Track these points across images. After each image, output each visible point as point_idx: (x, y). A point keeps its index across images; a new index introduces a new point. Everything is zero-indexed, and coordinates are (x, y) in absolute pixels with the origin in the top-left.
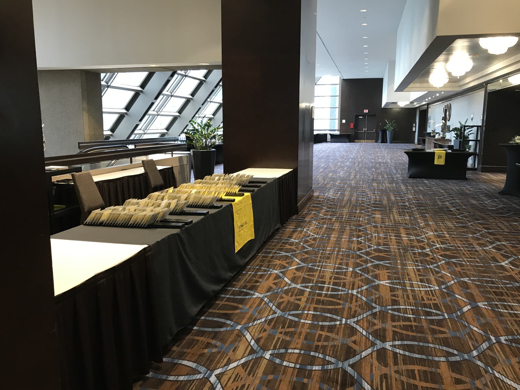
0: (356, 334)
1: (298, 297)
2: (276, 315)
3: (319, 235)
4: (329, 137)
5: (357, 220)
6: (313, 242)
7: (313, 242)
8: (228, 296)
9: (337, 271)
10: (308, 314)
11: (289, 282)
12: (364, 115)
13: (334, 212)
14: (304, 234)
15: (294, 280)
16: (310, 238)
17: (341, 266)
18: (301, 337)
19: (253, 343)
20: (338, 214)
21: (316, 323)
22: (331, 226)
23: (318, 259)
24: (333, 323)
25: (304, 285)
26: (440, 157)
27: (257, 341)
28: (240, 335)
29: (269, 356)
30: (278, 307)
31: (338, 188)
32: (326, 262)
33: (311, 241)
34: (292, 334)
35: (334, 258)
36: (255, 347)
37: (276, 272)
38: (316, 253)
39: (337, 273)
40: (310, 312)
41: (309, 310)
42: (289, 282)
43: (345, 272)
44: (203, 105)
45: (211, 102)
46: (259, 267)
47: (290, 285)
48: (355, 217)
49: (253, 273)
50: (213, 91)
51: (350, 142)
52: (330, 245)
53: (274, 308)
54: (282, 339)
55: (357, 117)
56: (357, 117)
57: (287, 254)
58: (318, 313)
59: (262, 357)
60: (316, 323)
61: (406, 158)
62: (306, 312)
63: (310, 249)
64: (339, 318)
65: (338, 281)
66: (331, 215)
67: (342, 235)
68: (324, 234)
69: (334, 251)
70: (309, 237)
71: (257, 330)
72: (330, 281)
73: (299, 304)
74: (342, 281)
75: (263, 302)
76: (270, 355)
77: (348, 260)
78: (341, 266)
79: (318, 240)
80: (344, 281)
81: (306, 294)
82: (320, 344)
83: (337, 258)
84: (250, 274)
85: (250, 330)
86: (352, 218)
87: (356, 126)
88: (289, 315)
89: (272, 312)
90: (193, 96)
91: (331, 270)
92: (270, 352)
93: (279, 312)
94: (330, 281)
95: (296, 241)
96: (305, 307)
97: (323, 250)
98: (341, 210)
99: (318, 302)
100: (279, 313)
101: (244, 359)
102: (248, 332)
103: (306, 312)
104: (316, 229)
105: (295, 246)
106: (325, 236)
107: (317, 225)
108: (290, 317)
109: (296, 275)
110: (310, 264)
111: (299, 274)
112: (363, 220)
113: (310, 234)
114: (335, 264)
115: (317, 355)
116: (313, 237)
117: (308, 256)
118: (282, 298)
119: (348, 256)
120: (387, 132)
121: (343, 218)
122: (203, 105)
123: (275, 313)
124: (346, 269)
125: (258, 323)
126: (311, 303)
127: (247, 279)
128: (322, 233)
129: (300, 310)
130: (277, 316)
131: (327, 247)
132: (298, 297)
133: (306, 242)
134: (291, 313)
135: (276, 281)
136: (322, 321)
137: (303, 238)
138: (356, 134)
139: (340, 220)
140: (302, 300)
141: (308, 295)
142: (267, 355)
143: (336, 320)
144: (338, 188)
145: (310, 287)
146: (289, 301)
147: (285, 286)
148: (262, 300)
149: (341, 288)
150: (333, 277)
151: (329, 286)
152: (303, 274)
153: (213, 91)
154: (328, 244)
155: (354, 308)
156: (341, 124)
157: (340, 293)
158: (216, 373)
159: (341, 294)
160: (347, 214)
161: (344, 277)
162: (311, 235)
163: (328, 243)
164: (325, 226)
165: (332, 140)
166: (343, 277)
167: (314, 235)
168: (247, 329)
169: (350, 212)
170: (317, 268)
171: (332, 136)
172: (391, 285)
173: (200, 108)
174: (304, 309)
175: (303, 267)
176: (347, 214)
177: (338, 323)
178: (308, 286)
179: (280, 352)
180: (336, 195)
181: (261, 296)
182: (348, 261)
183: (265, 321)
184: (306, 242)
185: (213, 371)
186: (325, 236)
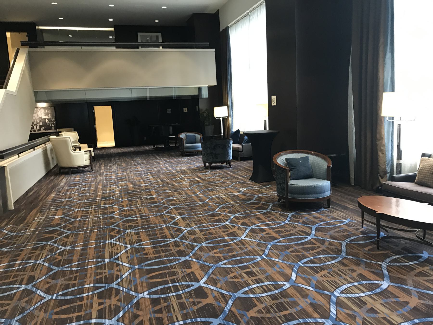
0: (46, 289)
1: (102, 307)
2: (115, 283)
5: (81, 209)
6: (111, 234)
7: (111, 234)
10: (88, 292)
13: (105, 213)
14: (126, 240)
16: (117, 237)
18: (89, 275)
19: (121, 263)
20: (100, 211)
21: (80, 287)
23: (102, 221)
24: (65, 291)
27: (118, 265)
30: (118, 291)
31: (112, 198)
32: (95, 220)
33: (114, 234)
34: (97, 274)
36: (117, 262)
38: (106, 224)
40: (86, 294)
41: (88, 296)
48: (83, 211)
52: (95, 234)
53: (121, 288)
54: (102, 270)
58: (78, 296)
59: (110, 259)
60: (80, 287)
62: (90, 293)
63: (112, 227)
64: (59, 298)
66: (106, 208)
67: (82, 250)
68: (107, 188)
69: (91, 230)
73: (99, 299)
77: (79, 225)
79: (107, 238)
82: (75, 275)
83: (88, 224)
86: (85, 209)
88: (105, 287)
89: (121, 284)
92: (106, 262)
93: (115, 286)
95: (128, 231)
96: (92, 298)
97: (100, 228)
98: (98, 216)
99: (80, 308)
100: (114, 285)
103: (90, 293)
105: (126, 225)
106: (102, 244)
108: (103, 285)
112: (75, 209)
117: (110, 221)
118: (119, 300)
119: (79, 228)
121: (95, 208)
125: (126, 273)
126: (87, 304)
128: (107, 247)
129: (96, 293)
131: (98, 231)
132: (102, 307)
134: (103, 289)
136: (74, 290)
139: (96, 205)
140: (97, 305)
141: (91, 313)
143: (62, 295)
144: (112, 198)
146: (110, 298)
147: (123, 316)
154: (97, 234)
155: (42, 313)
160: (91, 212)
163: (97, 235)
164: (107, 261)
167: (114, 242)
168: (130, 268)
169: (87, 216)
172: (166, 239)
174: (93, 295)
176: (91, 212)
177: (60, 293)
180: (110, 189)
183: (121, 276)
186: (102, 244)
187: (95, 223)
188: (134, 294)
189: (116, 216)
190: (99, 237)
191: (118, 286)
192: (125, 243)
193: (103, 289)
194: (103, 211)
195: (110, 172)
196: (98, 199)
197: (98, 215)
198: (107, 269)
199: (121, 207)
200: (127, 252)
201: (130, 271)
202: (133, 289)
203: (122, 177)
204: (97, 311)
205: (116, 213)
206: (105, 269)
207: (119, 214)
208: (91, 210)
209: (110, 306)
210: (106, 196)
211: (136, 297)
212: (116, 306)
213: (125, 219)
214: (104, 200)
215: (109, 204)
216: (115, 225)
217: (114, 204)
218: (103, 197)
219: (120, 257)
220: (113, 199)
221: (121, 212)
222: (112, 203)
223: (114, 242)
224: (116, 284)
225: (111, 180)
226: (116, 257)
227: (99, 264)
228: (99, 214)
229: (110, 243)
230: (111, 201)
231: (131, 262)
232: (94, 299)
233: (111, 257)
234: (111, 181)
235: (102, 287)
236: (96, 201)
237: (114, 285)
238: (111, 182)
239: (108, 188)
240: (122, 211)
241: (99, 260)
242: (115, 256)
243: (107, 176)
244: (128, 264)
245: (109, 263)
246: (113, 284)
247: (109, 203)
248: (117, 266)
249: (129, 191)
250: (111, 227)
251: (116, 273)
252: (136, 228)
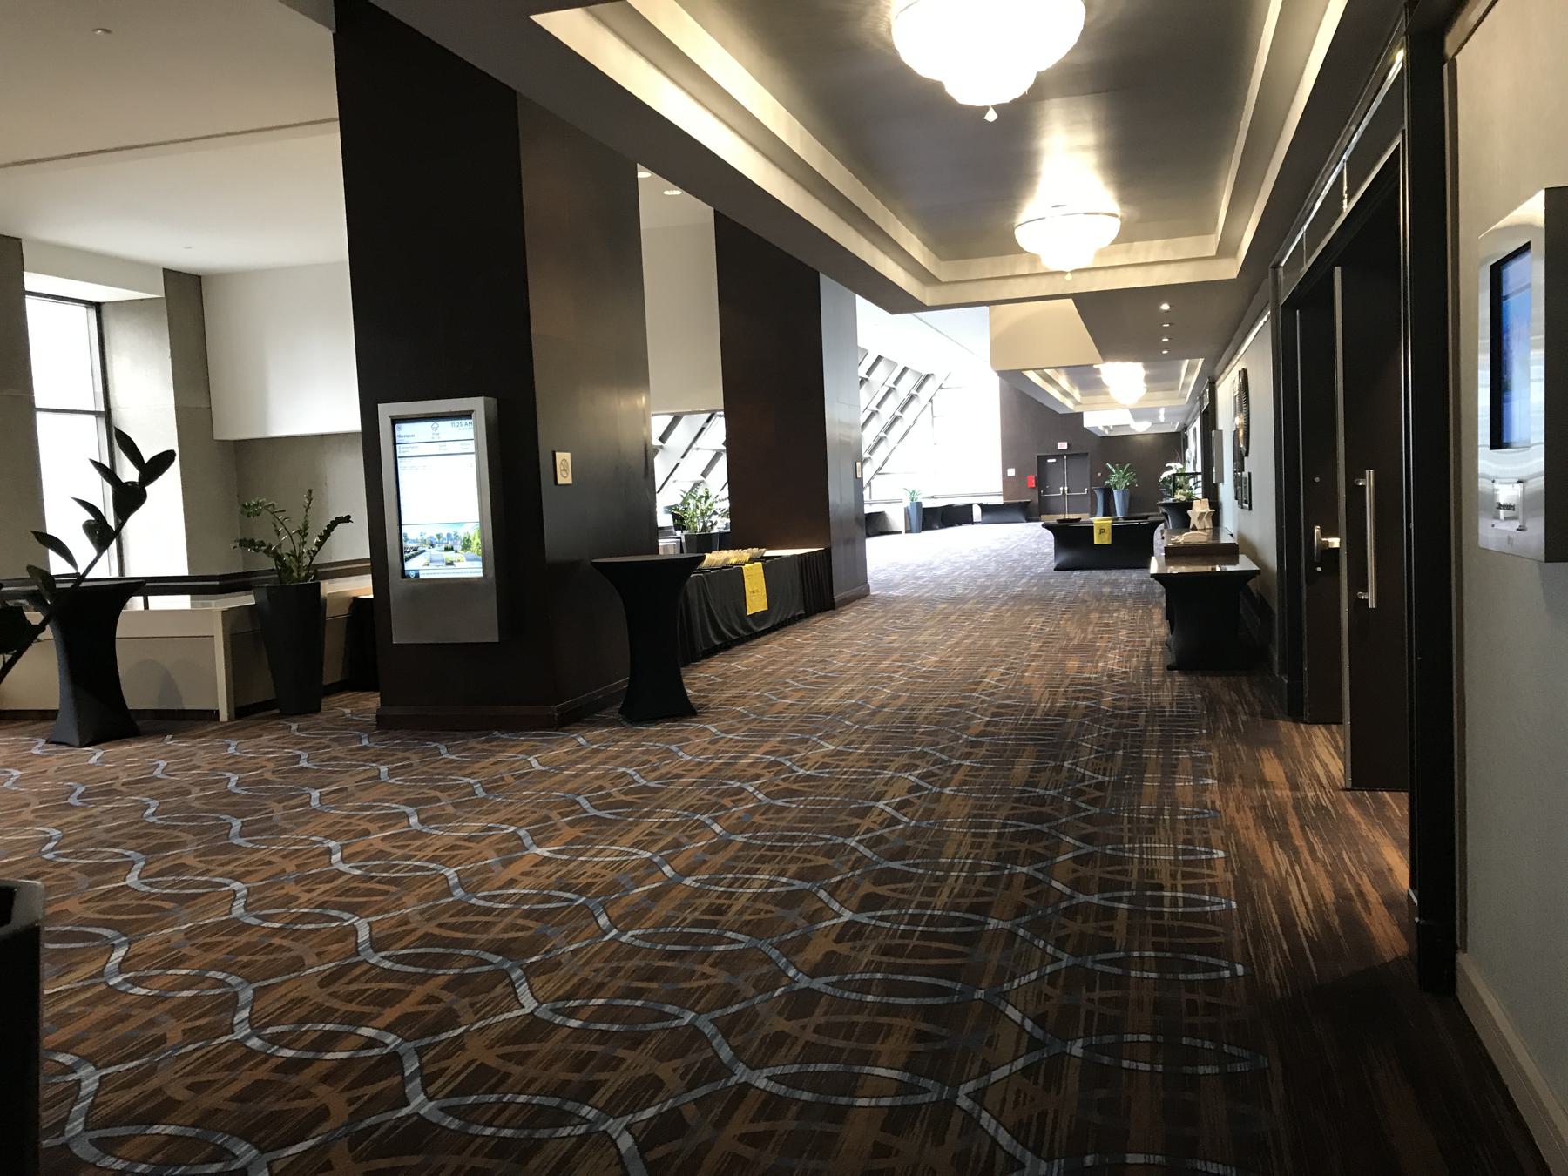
2: (1064, 965)
6: (1098, 794)
16: (1086, 783)
19: (1028, 1024)
23: (1126, 835)
27: (1039, 1021)
36: (1039, 1034)
53: (1050, 949)
68: (1122, 773)
88: (1095, 962)
89: (1048, 959)
92: (1080, 1043)
95: (1051, 793)
108: (1098, 967)
129: (1119, 951)
134: (1099, 957)
144: (1112, 730)
167: (1096, 776)
168: (1004, 996)
187: (1152, 831)
188: (1021, 932)
189: (1072, 841)
191: (1057, 955)
192: (971, 1121)
193: (1099, 957)
197: (1141, 860)
198: (1083, 1013)
199: (1039, 882)
200: (987, 1069)
201: (1006, 986)
202: (1018, 940)
206: (1090, 1014)
207: (1056, 848)
209: (1084, 922)
210: (1129, 738)
211: (1018, 926)
212: (1073, 919)
213: (1044, 828)
214: (1137, 726)
215: (1122, 716)
218: (1140, 736)
219: (1023, 1050)
220: (1110, 726)
221: (1048, 854)
222: (1070, 913)
223: (1096, 776)
224: (1061, 960)
225: (1121, 685)
226: (1035, 1056)
227: (1108, 1039)
229: (1044, 1153)
231: (991, 1013)
233: (1110, 758)
234: (1121, 682)
235: (1102, 962)
236: (1160, 726)
237: (1066, 960)
238: (1122, 679)
239: (1115, 771)
241: (1106, 1060)
242: (1038, 1064)
243: (1131, 704)
245: (1068, 1039)
246: (1070, 964)
247: (1122, 718)
248: (1045, 1015)
249: (1042, 745)
250: (1098, 810)
251: (1056, 992)
252: (1027, 795)
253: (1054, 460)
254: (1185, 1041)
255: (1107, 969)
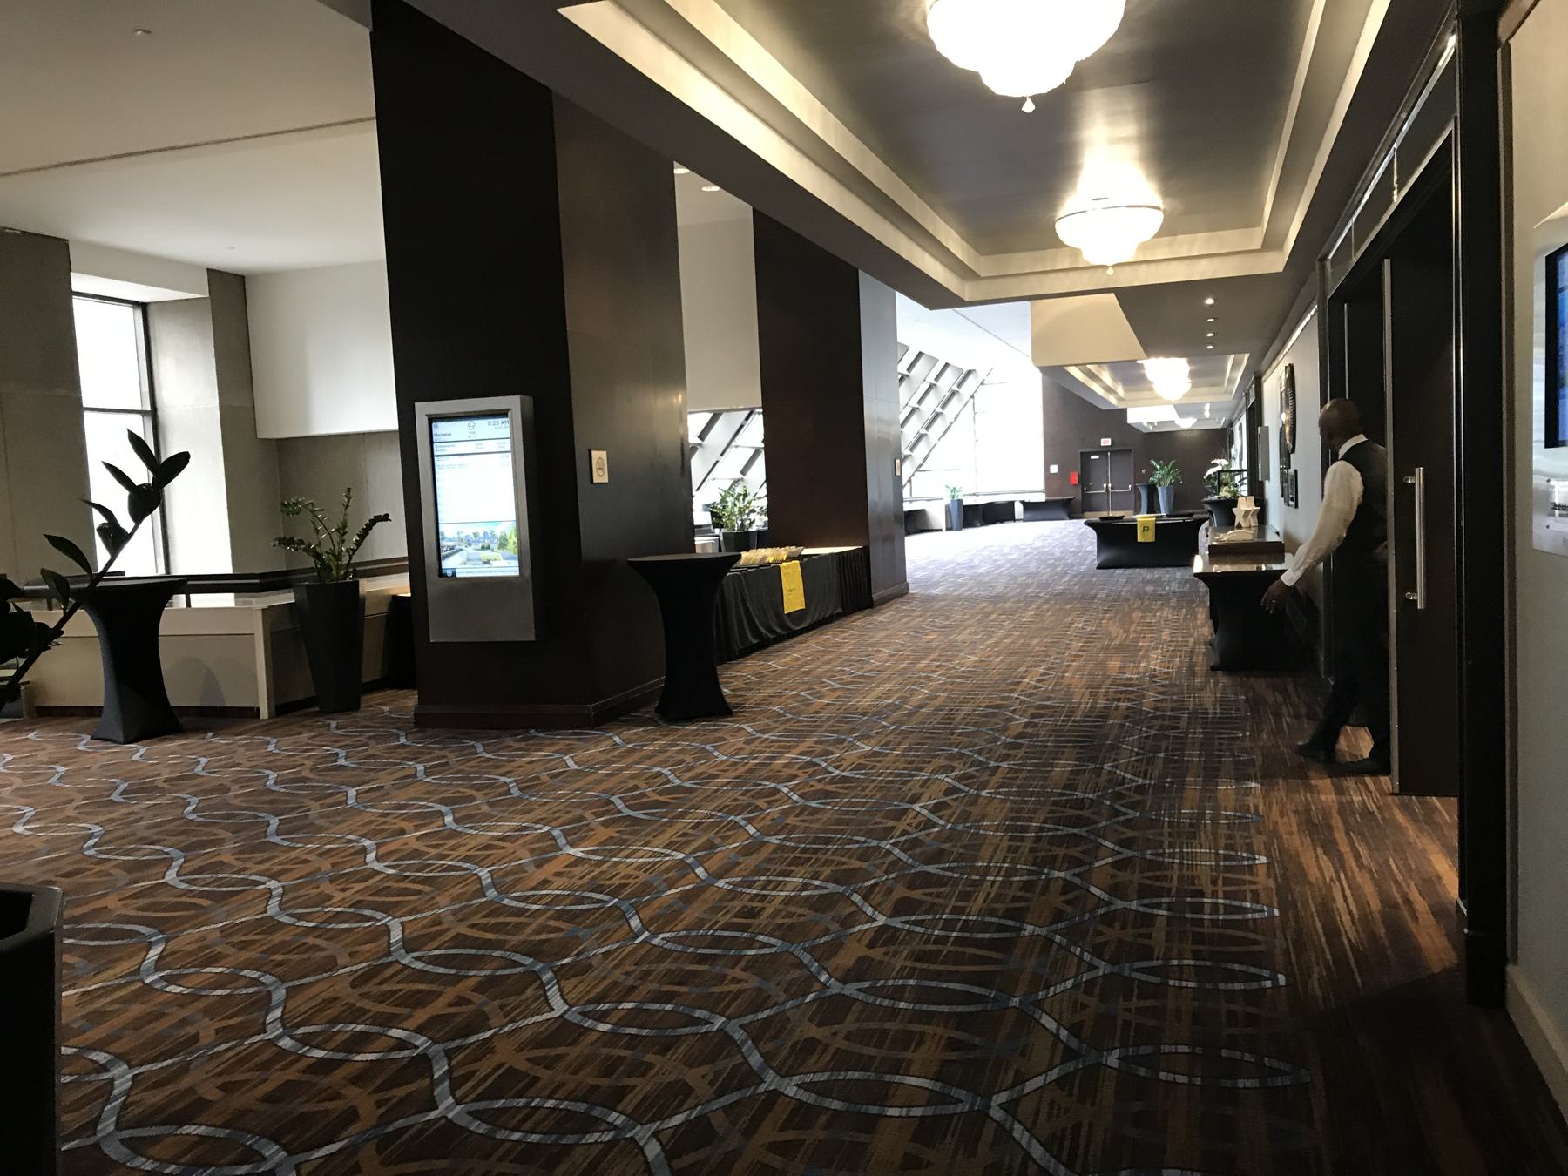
3: (1151, 779)
4: (1019, 509)
8: (954, 934)
9: (1227, 863)
11: (1106, 897)
12: (1103, 452)
15: (1116, 890)
16: (1126, 786)
17: (1233, 853)
19: (1064, 1033)
21: (1209, 986)
22: (1178, 755)
24: (1254, 985)
25: (1146, 901)
26: (1145, 529)
27: (1074, 1030)
28: (1026, 1021)
29: (1117, 1061)
30: (1098, 951)
35: (1207, 836)
36: (1074, 1043)
37: (1062, 874)
39: (1228, 869)
42: (1106, 897)
43: (1250, 866)
44: (722, 455)
45: (737, 447)
46: (1010, 862)
47: (1109, 904)
49: (1000, 879)
50: (742, 427)
51: (1071, 518)
53: (1086, 956)
54: (1137, 1024)
55: (1085, 456)
56: (1085, 456)
57: (1076, 831)
59: (1100, 1064)
61: (1092, 534)
64: (1266, 973)
65: (1233, 888)
68: (1163, 776)
69: (1202, 815)
70: (1124, 784)
71: (1064, 1006)
72: (1213, 888)
74: (1247, 887)
75: (1051, 946)
76: (1119, 1058)
78: (1233, 853)
80: (1254, 887)
81: (1161, 924)
84: (994, 882)
85: (1047, 1006)
87: (1084, 480)
88: (1132, 970)
89: (1084, 967)
90: (702, 439)
91: (1208, 863)
92: (1116, 1053)
94: (1213, 888)
95: (1091, 796)
100: (1103, 968)
101: (1056, 1071)
102: (1043, 1011)
104: (1136, 764)
105: (1090, 811)
107: (1137, 754)
108: (1136, 975)
109: (1118, 880)
110: (1149, 852)
111: (1122, 876)
113: (1124, 777)
114: (1217, 848)
115: (1238, 1055)
116: (1134, 784)
117: (1135, 834)
120: (1159, 489)
122: (722, 455)
123: (1092, 967)
124: (1248, 859)
125: (1058, 991)
127: (989, 894)
129: (1158, 959)
130: (1104, 975)
133: (1118, 796)
135: (1070, 896)
137: (1105, 788)
138: (1086, 497)
142: (1113, 1060)
144: (1153, 732)
145: (1164, 905)
146: (1120, 941)
148: (1049, 942)
149: (1249, 905)
150: (1220, 880)
151: (1214, 900)
152: (1136, 875)
153: (742, 427)
156: (1049, 477)
157: (1250, 916)
158: (999, 1102)
159: (1255, 920)
160: (1214, 883)
161: (1251, 879)
162: (1127, 781)
165: (1029, 515)
166: (1248, 877)
167: (1136, 779)
168: (1039, 1004)
170: (1171, 860)
171: (1027, 506)
173: (717, 462)
175: (1130, 859)
176: (1214, 883)
178: (1161, 904)
179: (1141, 1053)
181: (1043, 931)
182: (1248, 841)
184: (1118, 796)
185: (988, 1096)
187: (1193, 835)
190: (1174, 794)
191: (1094, 963)
192: (1003, 1133)
194: (1158, 879)
195: (1174, 644)
196: (1199, 733)
197: (1181, 864)
200: (1021, 1079)
201: (1041, 995)
203: (1121, 692)
204: (1154, 926)
205: (1109, 860)
206: (1127, 1023)
207: (1095, 852)
208: (1214, 894)
213: (1082, 831)
216: (1122, 818)
217: (1102, 911)
221: (1086, 858)
222: (1108, 919)
226: (1070, 1067)
227: (1146, 1050)
228: (1176, 867)
230: (1157, 723)
232: (1163, 949)
233: (1151, 761)
234: (1164, 682)
235: (1139, 970)
237: (1103, 968)
240: (1080, 863)
241: (1142, 1072)
243: (1174, 705)
244: (1038, 1021)
247: (1164, 720)
253: (1097, 457)
254: (1224, 1053)
255: (1144, 977)
